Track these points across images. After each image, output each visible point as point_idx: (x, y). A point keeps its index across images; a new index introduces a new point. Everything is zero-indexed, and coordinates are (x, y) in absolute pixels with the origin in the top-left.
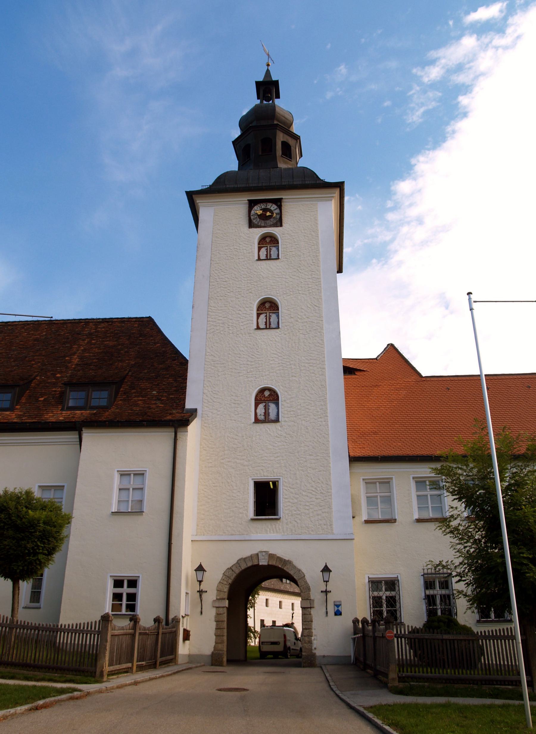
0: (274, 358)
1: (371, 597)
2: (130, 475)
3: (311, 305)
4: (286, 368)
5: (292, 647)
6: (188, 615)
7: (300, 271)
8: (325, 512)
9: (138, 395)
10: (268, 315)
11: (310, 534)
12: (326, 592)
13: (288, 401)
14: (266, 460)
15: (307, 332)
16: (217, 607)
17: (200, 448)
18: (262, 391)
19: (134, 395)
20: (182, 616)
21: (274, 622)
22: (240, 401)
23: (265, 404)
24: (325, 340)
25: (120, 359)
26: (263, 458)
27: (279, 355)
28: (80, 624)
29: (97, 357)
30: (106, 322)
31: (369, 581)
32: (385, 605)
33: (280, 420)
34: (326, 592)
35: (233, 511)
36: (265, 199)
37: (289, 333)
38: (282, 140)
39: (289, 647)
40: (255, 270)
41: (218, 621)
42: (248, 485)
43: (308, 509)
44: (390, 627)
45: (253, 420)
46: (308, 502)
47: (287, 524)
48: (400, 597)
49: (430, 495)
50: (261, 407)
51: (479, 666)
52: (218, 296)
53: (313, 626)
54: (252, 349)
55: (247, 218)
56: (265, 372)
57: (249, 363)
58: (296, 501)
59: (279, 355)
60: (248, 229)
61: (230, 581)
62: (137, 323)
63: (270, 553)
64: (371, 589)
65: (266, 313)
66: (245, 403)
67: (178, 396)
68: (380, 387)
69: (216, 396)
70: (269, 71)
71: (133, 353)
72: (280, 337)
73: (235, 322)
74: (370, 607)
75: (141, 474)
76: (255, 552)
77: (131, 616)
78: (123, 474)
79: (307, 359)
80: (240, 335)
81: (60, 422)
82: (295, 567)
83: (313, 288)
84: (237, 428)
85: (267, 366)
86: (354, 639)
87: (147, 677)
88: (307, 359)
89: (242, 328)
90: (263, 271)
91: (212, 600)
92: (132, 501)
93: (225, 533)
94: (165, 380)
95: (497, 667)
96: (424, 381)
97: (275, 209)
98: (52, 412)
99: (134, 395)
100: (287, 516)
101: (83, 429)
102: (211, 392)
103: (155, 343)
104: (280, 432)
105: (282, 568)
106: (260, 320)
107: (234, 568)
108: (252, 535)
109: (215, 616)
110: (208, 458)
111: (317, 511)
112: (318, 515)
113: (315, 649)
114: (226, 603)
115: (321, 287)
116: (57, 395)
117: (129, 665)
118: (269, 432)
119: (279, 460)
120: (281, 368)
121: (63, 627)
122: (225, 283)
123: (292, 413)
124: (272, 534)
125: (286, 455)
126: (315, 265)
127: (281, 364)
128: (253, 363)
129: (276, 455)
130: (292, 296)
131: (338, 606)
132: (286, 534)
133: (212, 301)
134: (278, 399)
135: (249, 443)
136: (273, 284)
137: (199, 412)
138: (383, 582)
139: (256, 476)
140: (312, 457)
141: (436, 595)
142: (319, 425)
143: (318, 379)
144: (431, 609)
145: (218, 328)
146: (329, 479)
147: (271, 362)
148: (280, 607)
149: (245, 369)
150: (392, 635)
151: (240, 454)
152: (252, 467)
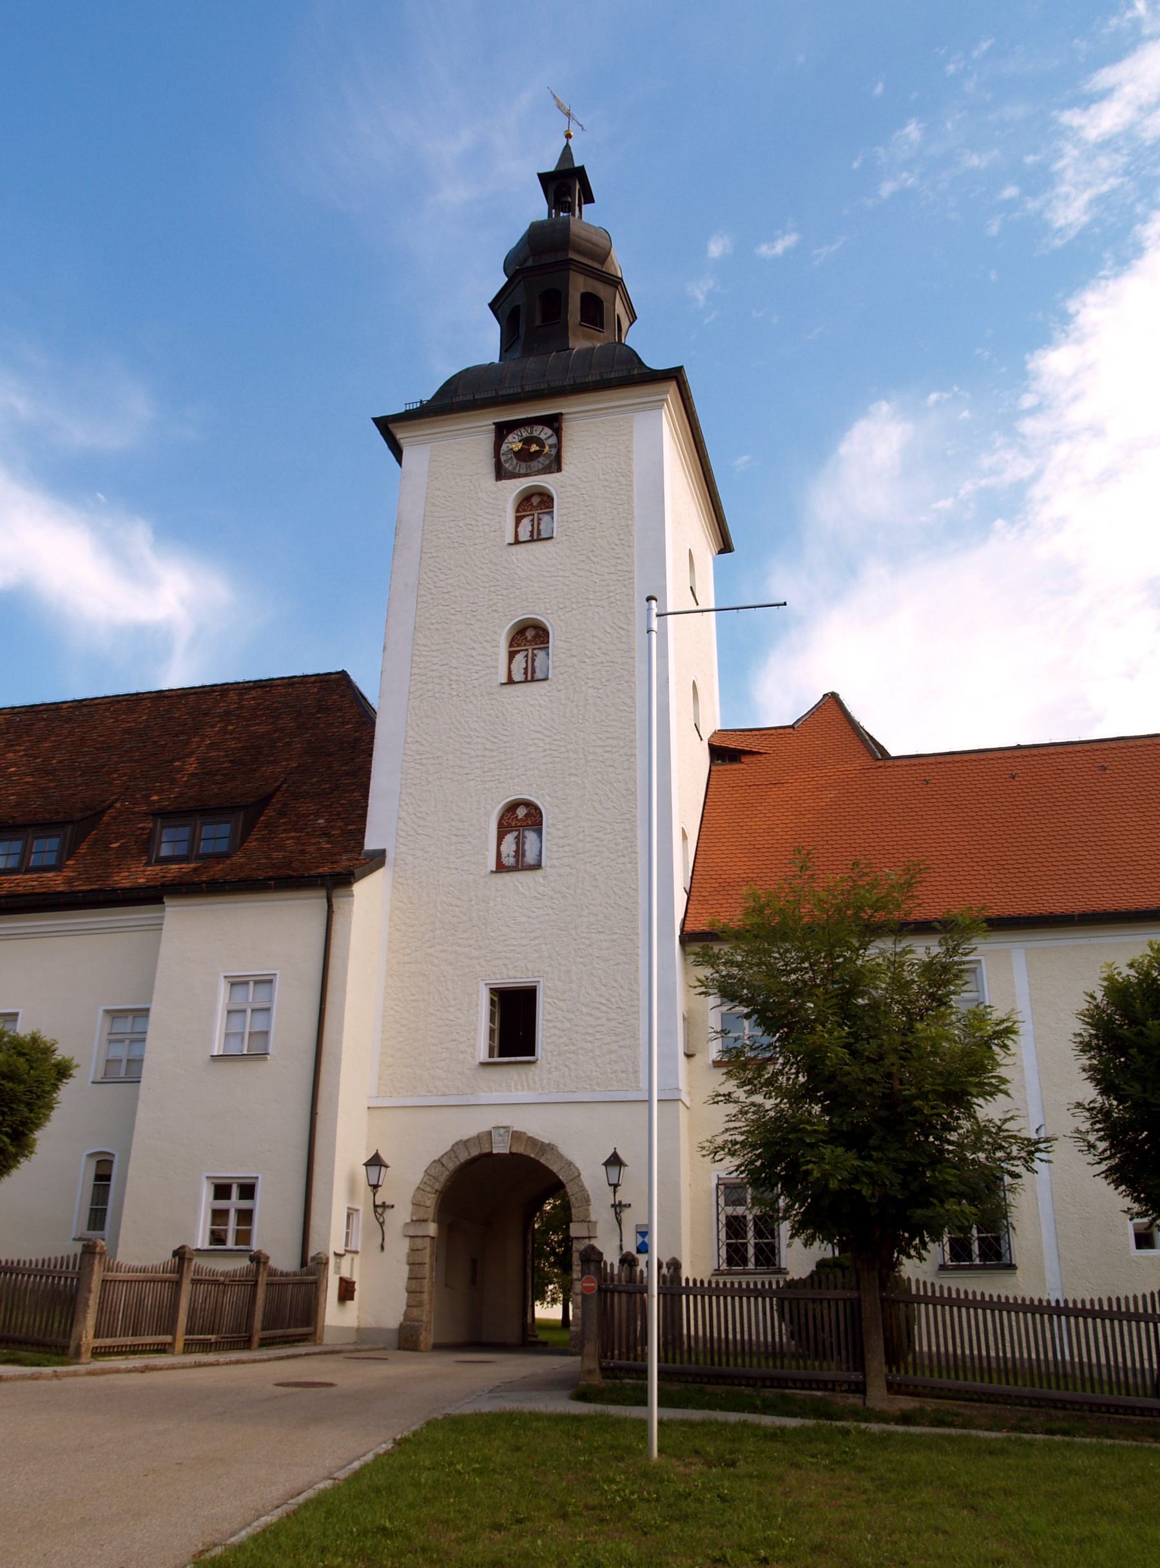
0: (536, 741)
2: (247, 983)
3: (611, 627)
4: (558, 759)
7: (592, 558)
11: (593, 1090)
13: (560, 826)
15: (602, 682)
16: (411, 1237)
17: (390, 927)
18: (512, 807)
19: (283, 827)
26: (507, 943)
27: (547, 733)
28: (50, 1259)
30: (260, 687)
31: (718, 1185)
33: (543, 865)
35: (447, 1048)
37: (566, 688)
38: (582, 290)
40: (506, 565)
42: (477, 996)
47: (549, 1072)
50: (510, 839)
51: (910, 1358)
56: (517, 770)
57: (487, 753)
58: (569, 1025)
59: (547, 733)
61: (438, 1186)
66: (478, 834)
73: (462, 672)
75: (266, 982)
78: (236, 983)
81: (139, 888)
82: (561, 1157)
83: (618, 591)
84: (460, 884)
85: (522, 758)
88: (600, 738)
89: (476, 683)
91: (402, 1223)
92: (251, 1034)
93: (430, 1092)
95: (955, 1361)
97: (549, 437)
99: (283, 827)
100: (549, 1055)
101: (165, 900)
102: (413, 816)
103: (343, 723)
104: (541, 889)
106: (513, 666)
107: (444, 1161)
108: (482, 1094)
110: (404, 945)
112: (611, 1052)
114: (432, 1229)
115: (633, 588)
117: (168, 1338)
119: (539, 945)
120: (548, 759)
121: (21, 1265)
122: (447, 596)
123: (566, 849)
124: (520, 1093)
128: (494, 754)
129: (532, 935)
130: (574, 612)
132: (546, 1091)
135: (481, 913)
139: (493, 977)
140: (602, 937)
142: (618, 871)
143: (620, 777)
145: (430, 686)
147: (530, 749)
149: (478, 765)
151: (465, 935)
152: (487, 961)
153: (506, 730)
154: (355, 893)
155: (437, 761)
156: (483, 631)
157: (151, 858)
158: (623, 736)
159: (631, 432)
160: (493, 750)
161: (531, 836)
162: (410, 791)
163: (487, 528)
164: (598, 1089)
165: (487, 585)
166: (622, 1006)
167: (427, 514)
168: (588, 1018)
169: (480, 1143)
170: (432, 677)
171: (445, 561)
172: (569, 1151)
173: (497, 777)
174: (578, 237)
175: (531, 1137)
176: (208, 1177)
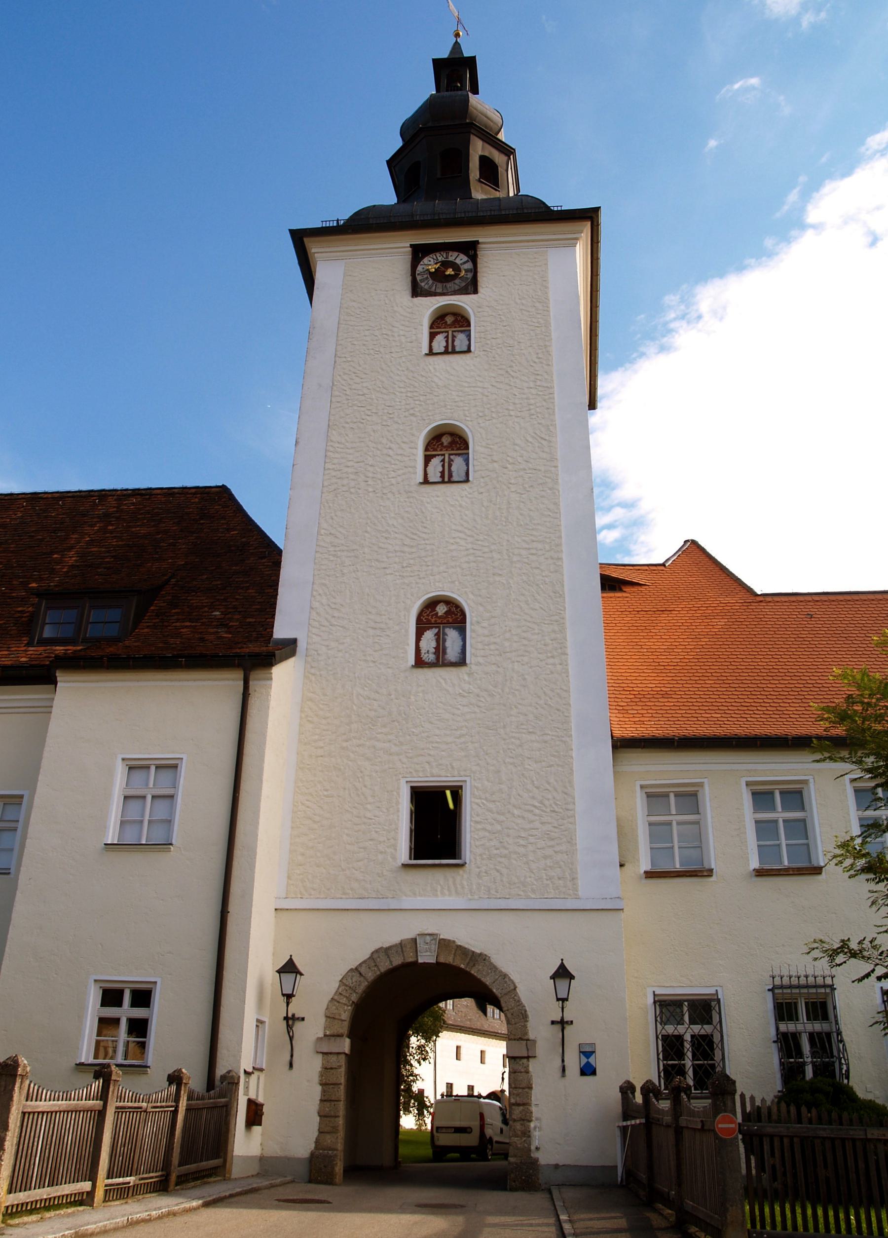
0: (458, 540)
1: (660, 1037)
2: (148, 767)
3: (533, 437)
5: (495, 1139)
6: (261, 1070)
8: (561, 852)
9: (184, 617)
10: (447, 460)
12: (563, 1023)
14: (437, 742)
15: (525, 488)
16: (323, 1053)
17: (301, 718)
18: (431, 605)
19: (175, 617)
20: (245, 1071)
21: (471, 1088)
22: (386, 624)
23: (437, 630)
24: (561, 504)
25: (157, 556)
29: (114, 554)
30: (138, 494)
31: (655, 1002)
32: (689, 1054)
33: (468, 661)
34: (563, 1023)
35: (365, 848)
36: (445, 243)
38: (480, 153)
39: (491, 1138)
41: (326, 1085)
42: (398, 794)
43: (524, 846)
44: (725, 1105)
45: (412, 660)
46: (525, 830)
47: (479, 876)
48: (722, 1036)
49: (784, 821)
50: (429, 636)
52: (347, 423)
53: (533, 1099)
54: (412, 521)
55: (410, 279)
58: (499, 828)
60: (410, 298)
61: (354, 997)
62: (198, 496)
63: (442, 937)
64: (658, 1019)
65: (444, 455)
66: (397, 628)
67: (263, 620)
68: (673, 612)
69: (336, 614)
70: (459, 44)
71: (184, 546)
72: (470, 498)
73: (379, 470)
74: (658, 1059)
75: (173, 767)
76: (409, 935)
77: (97, 1068)
78: (134, 767)
79: (524, 541)
80: (390, 495)
82: (494, 968)
83: (538, 405)
86: (624, 1129)
87: (121, 1220)
88: (524, 541)
89: (393, 481)
90: (437, 374)
91: (314, 1038)
92: (150, 822)
93: (344, 894)
94: (240, 591)
96: (761, 601)
97: (465, 263)
98: (8, 648)
99: (175, 617)
102: (326, 607)
104: (466, 687)
105: (467, 969)
106: (430, 469)
108: (404, 898)
109: (321, 1072)
110: (316, 737)
111: (543, 848)
112: (545, 857)
113: (537, 1149)
114: (346, 1045)
116: (24, 619)
117: (86, 1186)
118: (444, 684)
119: (464, 743)
120: (471, 558)
122: (363, 398)
123: (492, 647)
125: (478, 733)
126: (541, 363)
127: (472, 551)
128: (414, 550)
129: (459, 732)
130: (494, 421)
131: (588, 1054)
132: (476, 897)
133: (334, 432)
134: (464, 620)
136: (457, 399)
137: (301, 646)
138: (686, 1003)
139: (415, 775)
141: (800, 1033)
144: (791, 1063)
145: (345, 482)
146: (571, 782)
147: (453, 547)
148: (482, 1061)
149: (397, 560)
150: (733, 1126)
153: (425, 527)
154: (274, 676)
155: (353, 554)
156: (400, 433)
157: (34, 640)
158: (548, 540)
159: (546, 264)
160: (412, 547)
161: (452, 636)
162: (324, 581)
163: (403, 339)
164: (533, 896)
165: (403, 390)
166: (557, 809)
167: (341, 322)
168: (519, 821)
169: (402, 951)
170: (346, 473)
171: (360, 366)
172: (502, 961)
173: (416, 573)
174: (476, 109)
175: (460, 946)
176: (95, 981)
